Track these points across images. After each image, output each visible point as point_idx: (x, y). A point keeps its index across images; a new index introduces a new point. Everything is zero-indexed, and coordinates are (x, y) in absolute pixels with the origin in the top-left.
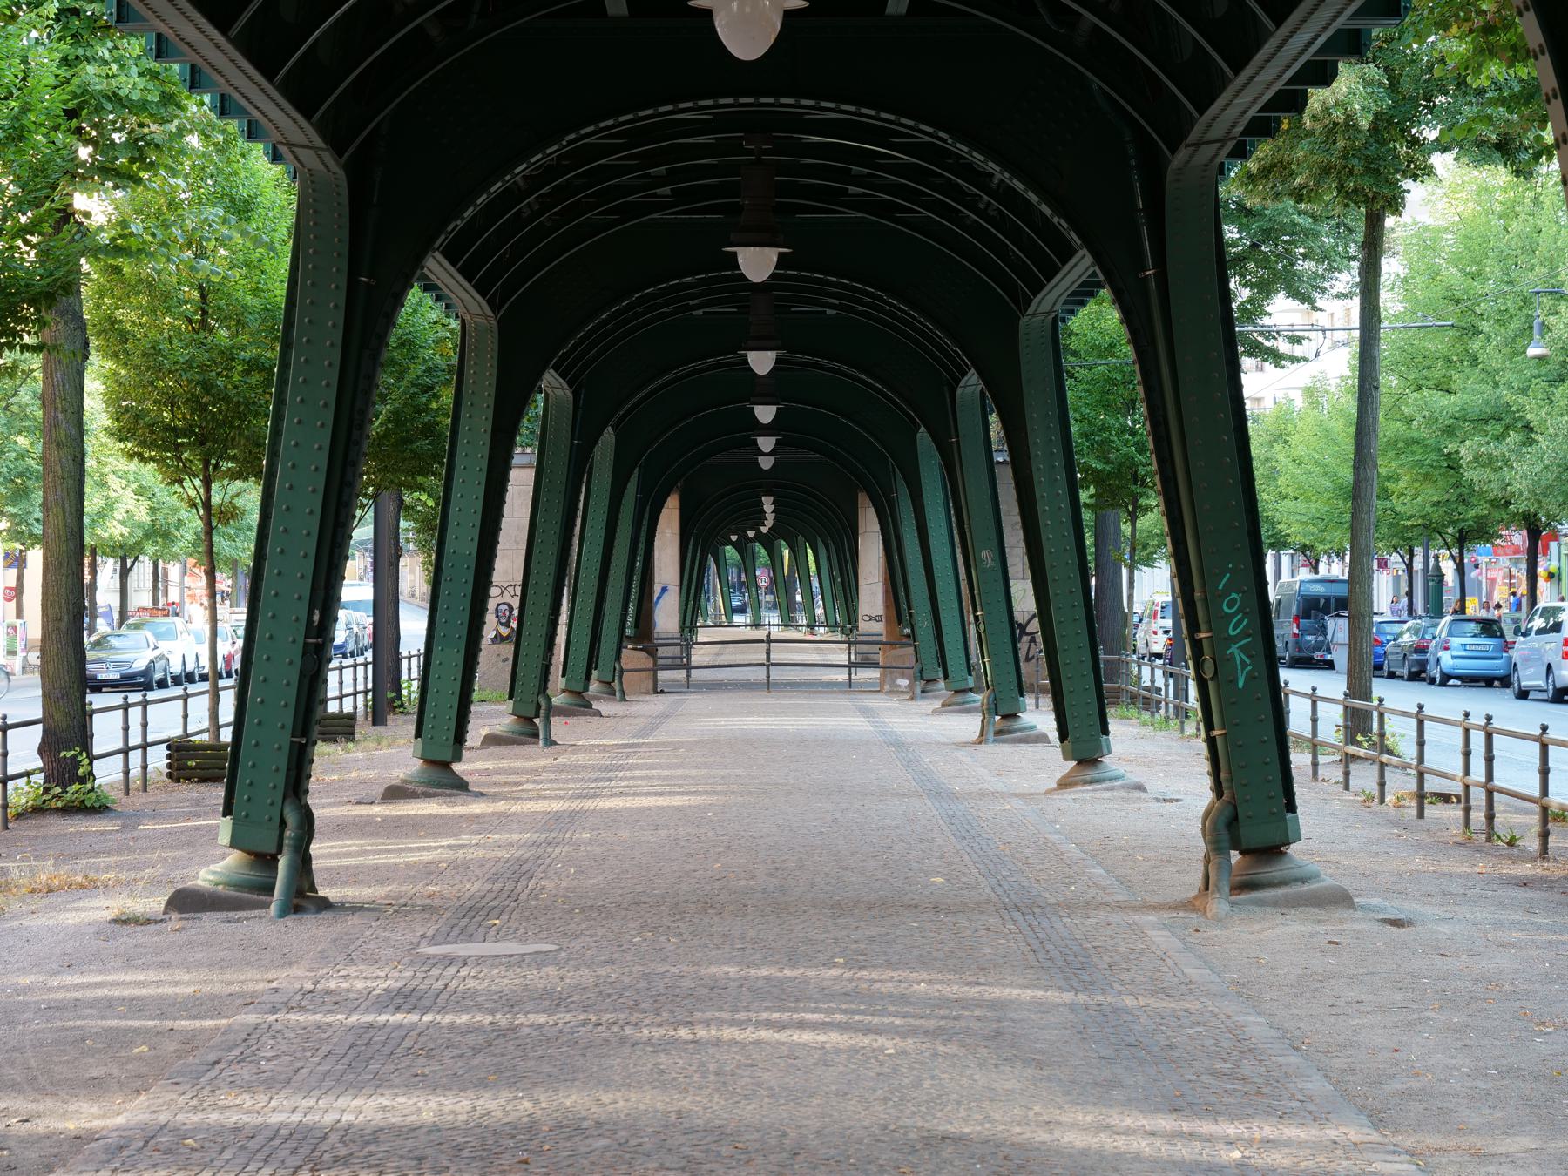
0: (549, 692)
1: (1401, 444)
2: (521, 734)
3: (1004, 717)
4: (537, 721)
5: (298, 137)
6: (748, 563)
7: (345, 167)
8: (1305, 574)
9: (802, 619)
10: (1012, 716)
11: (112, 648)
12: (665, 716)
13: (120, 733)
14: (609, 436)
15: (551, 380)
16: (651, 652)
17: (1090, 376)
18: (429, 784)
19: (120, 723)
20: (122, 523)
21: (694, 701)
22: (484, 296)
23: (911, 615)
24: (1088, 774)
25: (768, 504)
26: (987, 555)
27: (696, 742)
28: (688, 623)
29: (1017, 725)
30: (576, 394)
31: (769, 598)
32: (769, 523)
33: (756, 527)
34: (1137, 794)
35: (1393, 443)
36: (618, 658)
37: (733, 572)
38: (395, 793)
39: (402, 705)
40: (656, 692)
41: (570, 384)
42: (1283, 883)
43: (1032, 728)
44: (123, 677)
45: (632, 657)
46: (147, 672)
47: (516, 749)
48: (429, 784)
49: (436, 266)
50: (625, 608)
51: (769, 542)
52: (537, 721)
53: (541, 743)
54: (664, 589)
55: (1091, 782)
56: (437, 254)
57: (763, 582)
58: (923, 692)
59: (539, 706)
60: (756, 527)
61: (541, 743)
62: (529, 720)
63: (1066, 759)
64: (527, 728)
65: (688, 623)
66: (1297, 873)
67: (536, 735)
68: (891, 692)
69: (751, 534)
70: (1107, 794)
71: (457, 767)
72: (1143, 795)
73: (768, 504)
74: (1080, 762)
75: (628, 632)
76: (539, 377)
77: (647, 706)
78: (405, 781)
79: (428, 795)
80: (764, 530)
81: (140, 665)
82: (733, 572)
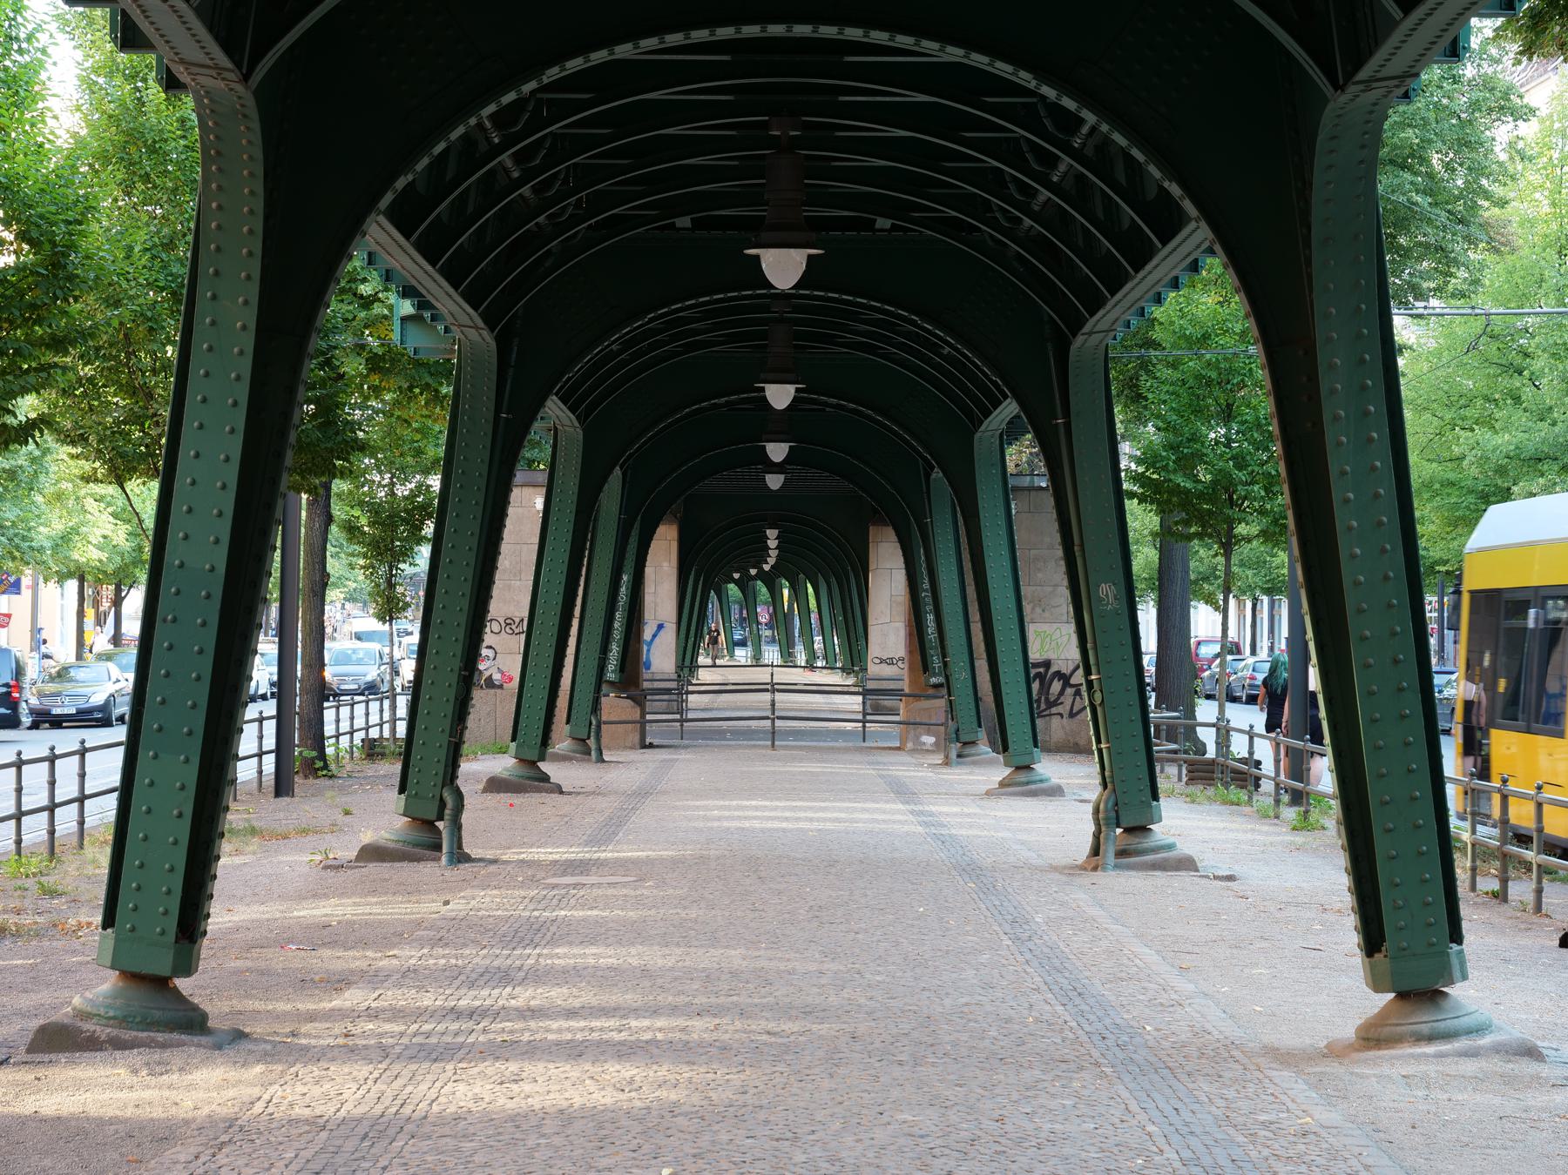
0: (459, 782)
1: (1437, 486)
2: (416, 845)
3: (1128, 830)
4: (440, 825)
5: (465, 320)
6: (749, 600)
7: (497, 339)
8: (409, 613)
9: (801, 659)
10: (1142, 829)
11: (71, 680)
12: (642, 794)
13: (76, 779)
14: (617, 471)
15: (555, 409)
16: (639, 700)
17: (1177, 375)
18: (124, 1021)
19: (45, 777)
20: (100, 548)
21: (688, 767)
22: (476, 309)
23: (945, 664)
24: (1424, 1020)
25: (772, 538)
26: (1107, 592)
27: (675, 863)
28: (687, 662)
29: (1149, 842)
30: (503, 343)
31: (768, 633)
32: (772, 561)
33: (758, 565)
34: (1528, 1067)
35: (1427, 485)
36: (596, 707)
37: (735, 608)
38: (58, 1041)
39: (326, 767)
40: (644, 746)
41: (490, 321)
42: (1034, 782)
43: (1170, 847)
44: (80, 712)
45: (614, 706)
46: (105, 708)
47: (405, 871)
48: (124, 1021)
49: (379, 233)
50: (605, 649)
51: (770, 581)
52: (440, 825)
53: (444, 859)
54: (660, 627)
55: (1431, 1038)
56: (381, 219)
57: (764, 618)
58: (959, 756)
59: (442, 804)
60: (758, 565)
61: (444, 859)
62: (429, 825)
63: (1377, 989)
64: (424, 837)
65: (687, 662)
66: (1464, 1022)
67: (437, 847)
68: (914, 751)
69: (753, 572)
70: (1470, 1067)
71: (182, 984)
72: (1544, 1070)
73: (772, 538)
74: (1402, 996)
75: (611, 675)
76: (541, 403)
77: (628, 769)
78: (82, 1015)
79: (119, 1045)
80: (766, 567)
81: (98, 699)
82: (735, 608)
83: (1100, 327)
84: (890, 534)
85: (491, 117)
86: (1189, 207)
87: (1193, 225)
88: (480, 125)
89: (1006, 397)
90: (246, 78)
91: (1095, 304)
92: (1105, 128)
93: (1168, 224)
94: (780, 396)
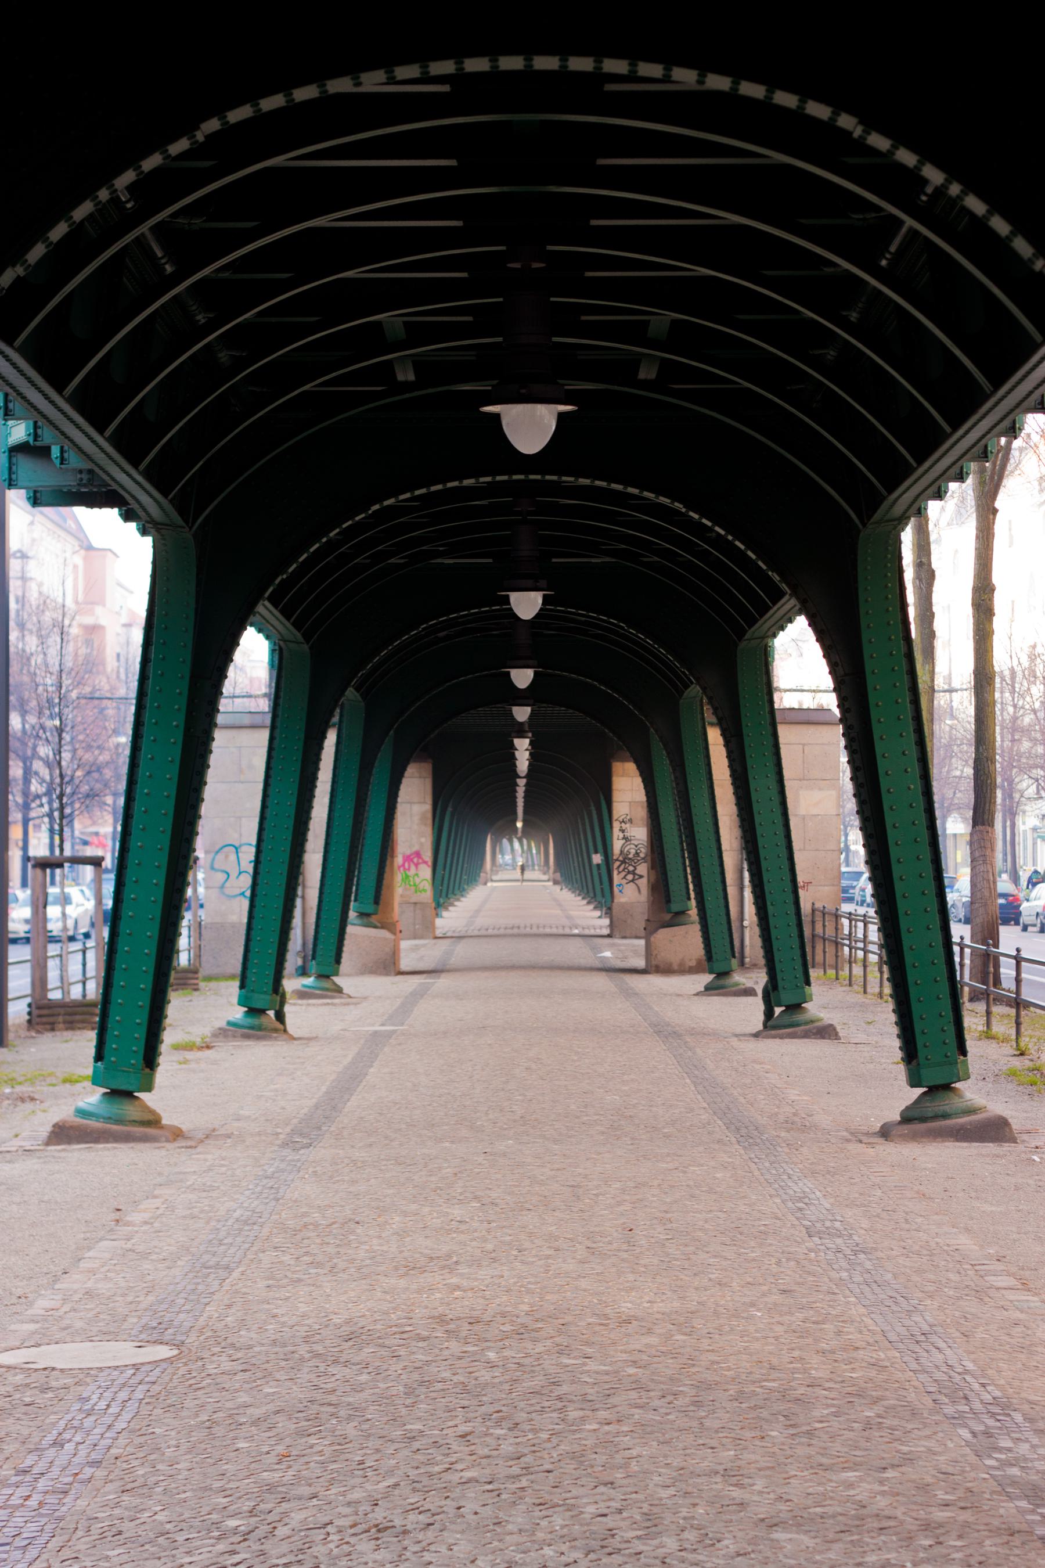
50: (581, 845)
56: (266, 603)
83: (756, 635)
84: (631, 767)
85: (130, 188)
86: (784, 587)
87: (787, 597)
88: (115, 200)
89: (692, 683)
90: (191, 528)
91: (752, 622)
92: (955, 189)
93: (777, 596)
94: (527, 604)
